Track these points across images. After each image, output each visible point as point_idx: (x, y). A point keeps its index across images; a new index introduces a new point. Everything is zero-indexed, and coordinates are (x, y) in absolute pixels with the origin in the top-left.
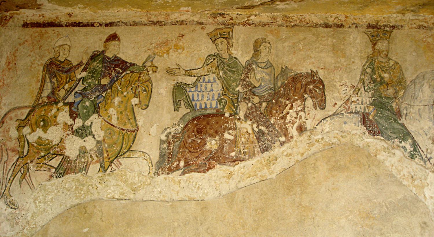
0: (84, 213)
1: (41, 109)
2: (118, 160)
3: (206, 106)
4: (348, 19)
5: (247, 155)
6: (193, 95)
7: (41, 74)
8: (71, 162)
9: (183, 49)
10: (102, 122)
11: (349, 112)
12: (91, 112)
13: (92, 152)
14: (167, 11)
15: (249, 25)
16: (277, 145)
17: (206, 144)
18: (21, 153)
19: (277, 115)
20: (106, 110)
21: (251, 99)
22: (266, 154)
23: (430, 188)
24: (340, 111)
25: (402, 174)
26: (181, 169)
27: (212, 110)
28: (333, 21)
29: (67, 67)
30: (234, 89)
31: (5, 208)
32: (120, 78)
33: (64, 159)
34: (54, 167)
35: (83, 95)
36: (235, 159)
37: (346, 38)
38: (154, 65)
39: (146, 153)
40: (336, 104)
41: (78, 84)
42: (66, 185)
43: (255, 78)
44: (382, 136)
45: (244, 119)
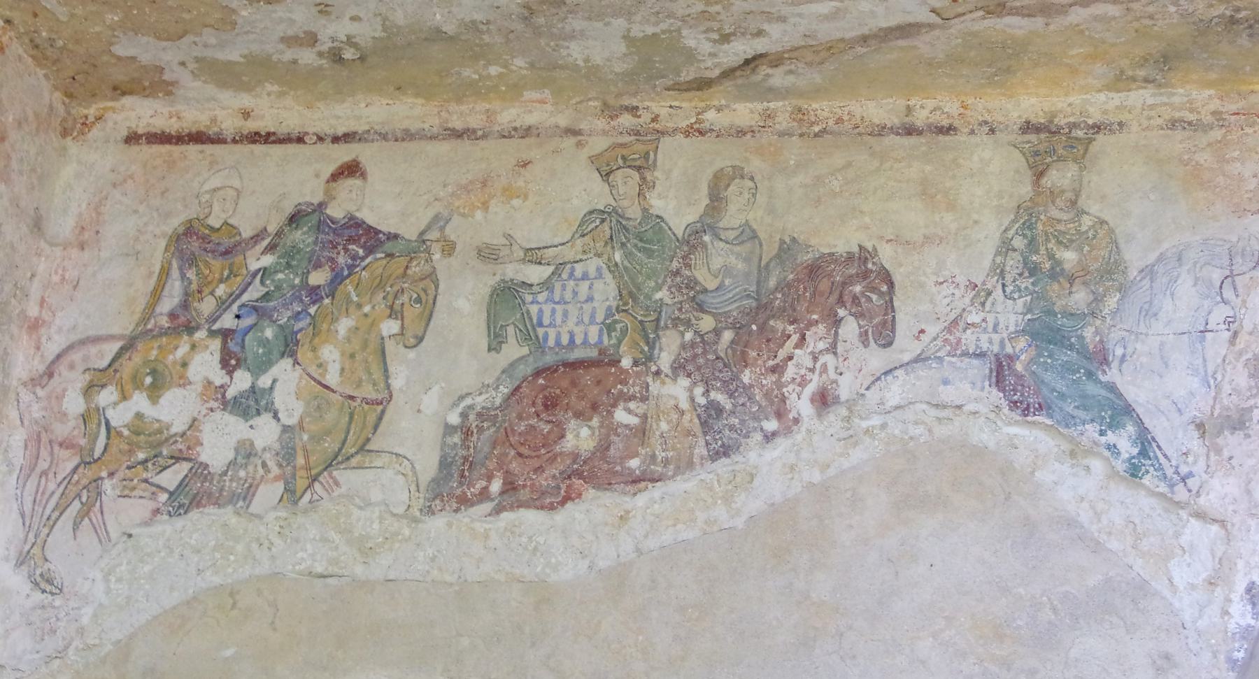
0: (229, 607)
3: (572, 341)
4: (968, 112)
5: (672, 467)
6: (541, 311)
8: (212, 479)
9: (526, 197)
10: (301, 378)
11: (959, 352)
12: (276, 354)
13: (267, 456)
17: (563, 436)
18: (85, 453)
20: (314, 350)
21: (694, 321)
22: (723, 465)
23: (1189, 560)
25: (1105, 521)
26: (492, 500)
27: (589, 350)
28: (928, 118)
29: (227, 242)
30: (648, 297)
31: (28, 591)
32: (358, 269)
33: (194, 471)
36: (638, 476)
38: (447, 239)
39: (405, 457)
40: (922, 331)
42: (191, 538)
43: (706, 267)
44: (1050, 416)
45: (670, 374)
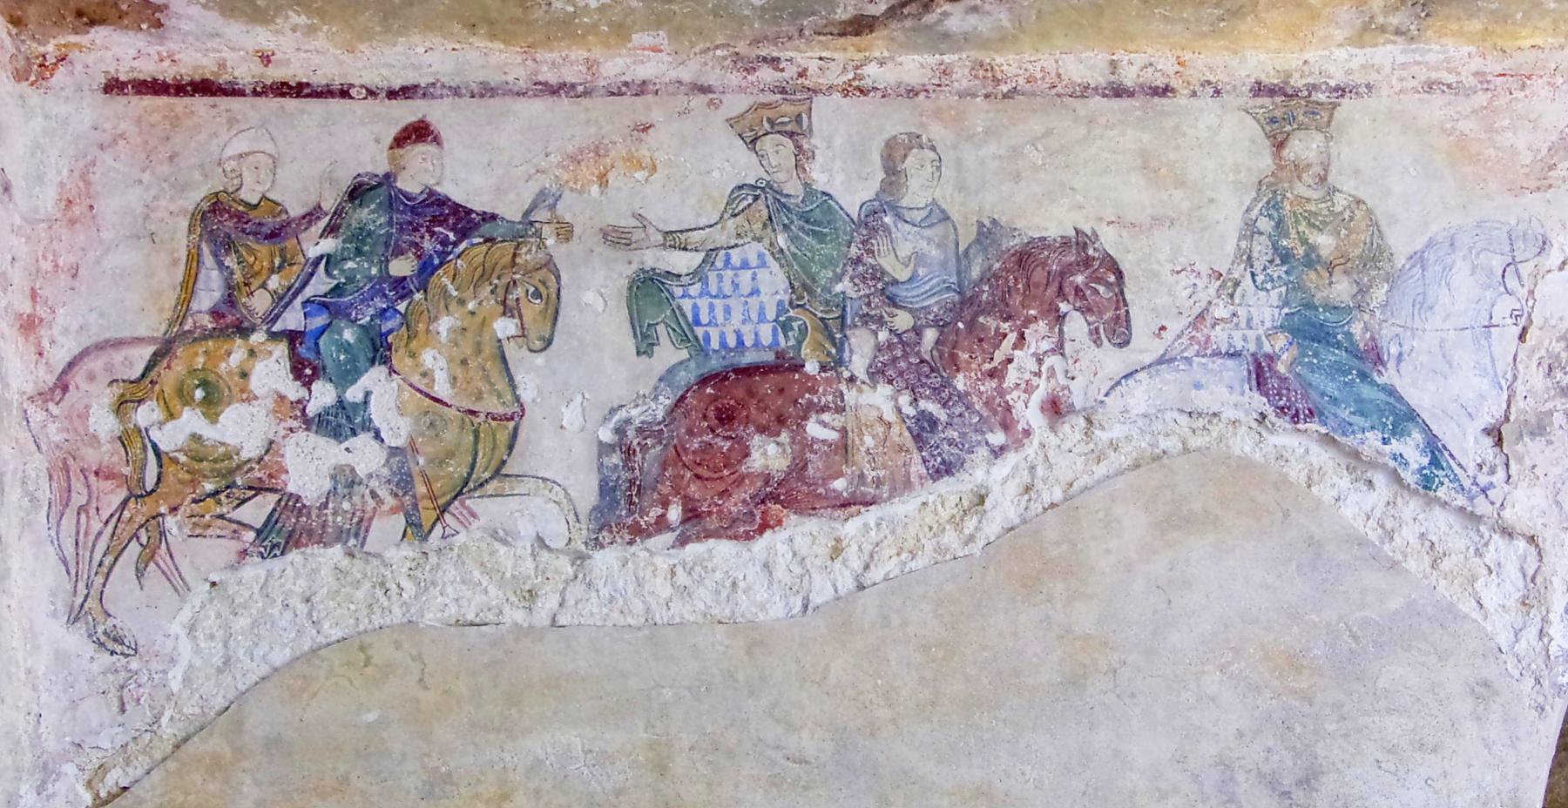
1: (195, 350)
2: (463, 504)
5: (886, 488)
6: (695, 307)
7: (185, 242)
10: (400, 388)
11: (1209, 352)
12: (362, 363)
14: (589, 50)
15: (863, 92)
16: (981, 458)
17: (747, 455)
19: (974, 366)
20: (413, 355)
21: (887, 318)
22: (946, 485)
24: (1178, 350)
26: (673, 530)
29: (271, 222)
30: (827, 290)
33: (283, 503)
34: (252, 528)
35: (331, 308)
37: (1185, 129)
40: (1163, 328)
41: (312, 275)
43: (893, 255)
